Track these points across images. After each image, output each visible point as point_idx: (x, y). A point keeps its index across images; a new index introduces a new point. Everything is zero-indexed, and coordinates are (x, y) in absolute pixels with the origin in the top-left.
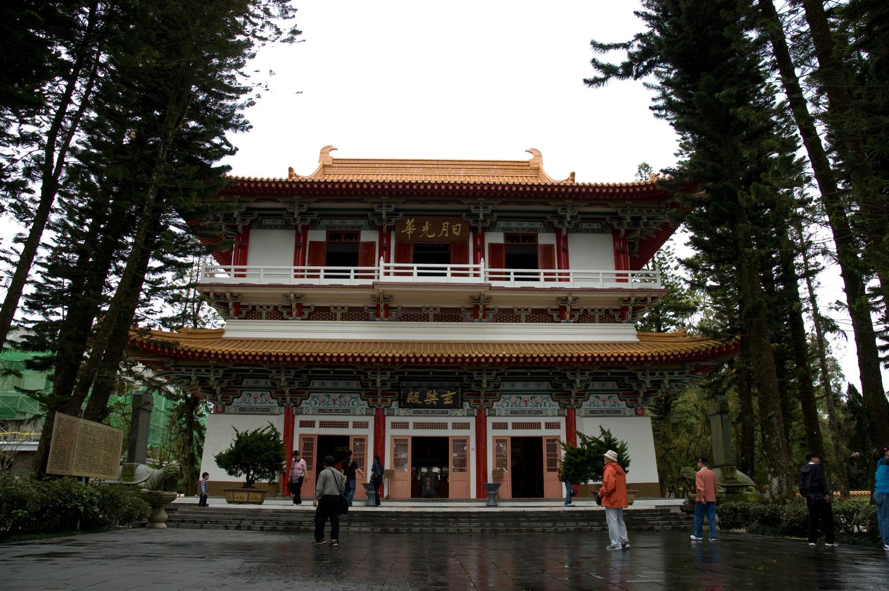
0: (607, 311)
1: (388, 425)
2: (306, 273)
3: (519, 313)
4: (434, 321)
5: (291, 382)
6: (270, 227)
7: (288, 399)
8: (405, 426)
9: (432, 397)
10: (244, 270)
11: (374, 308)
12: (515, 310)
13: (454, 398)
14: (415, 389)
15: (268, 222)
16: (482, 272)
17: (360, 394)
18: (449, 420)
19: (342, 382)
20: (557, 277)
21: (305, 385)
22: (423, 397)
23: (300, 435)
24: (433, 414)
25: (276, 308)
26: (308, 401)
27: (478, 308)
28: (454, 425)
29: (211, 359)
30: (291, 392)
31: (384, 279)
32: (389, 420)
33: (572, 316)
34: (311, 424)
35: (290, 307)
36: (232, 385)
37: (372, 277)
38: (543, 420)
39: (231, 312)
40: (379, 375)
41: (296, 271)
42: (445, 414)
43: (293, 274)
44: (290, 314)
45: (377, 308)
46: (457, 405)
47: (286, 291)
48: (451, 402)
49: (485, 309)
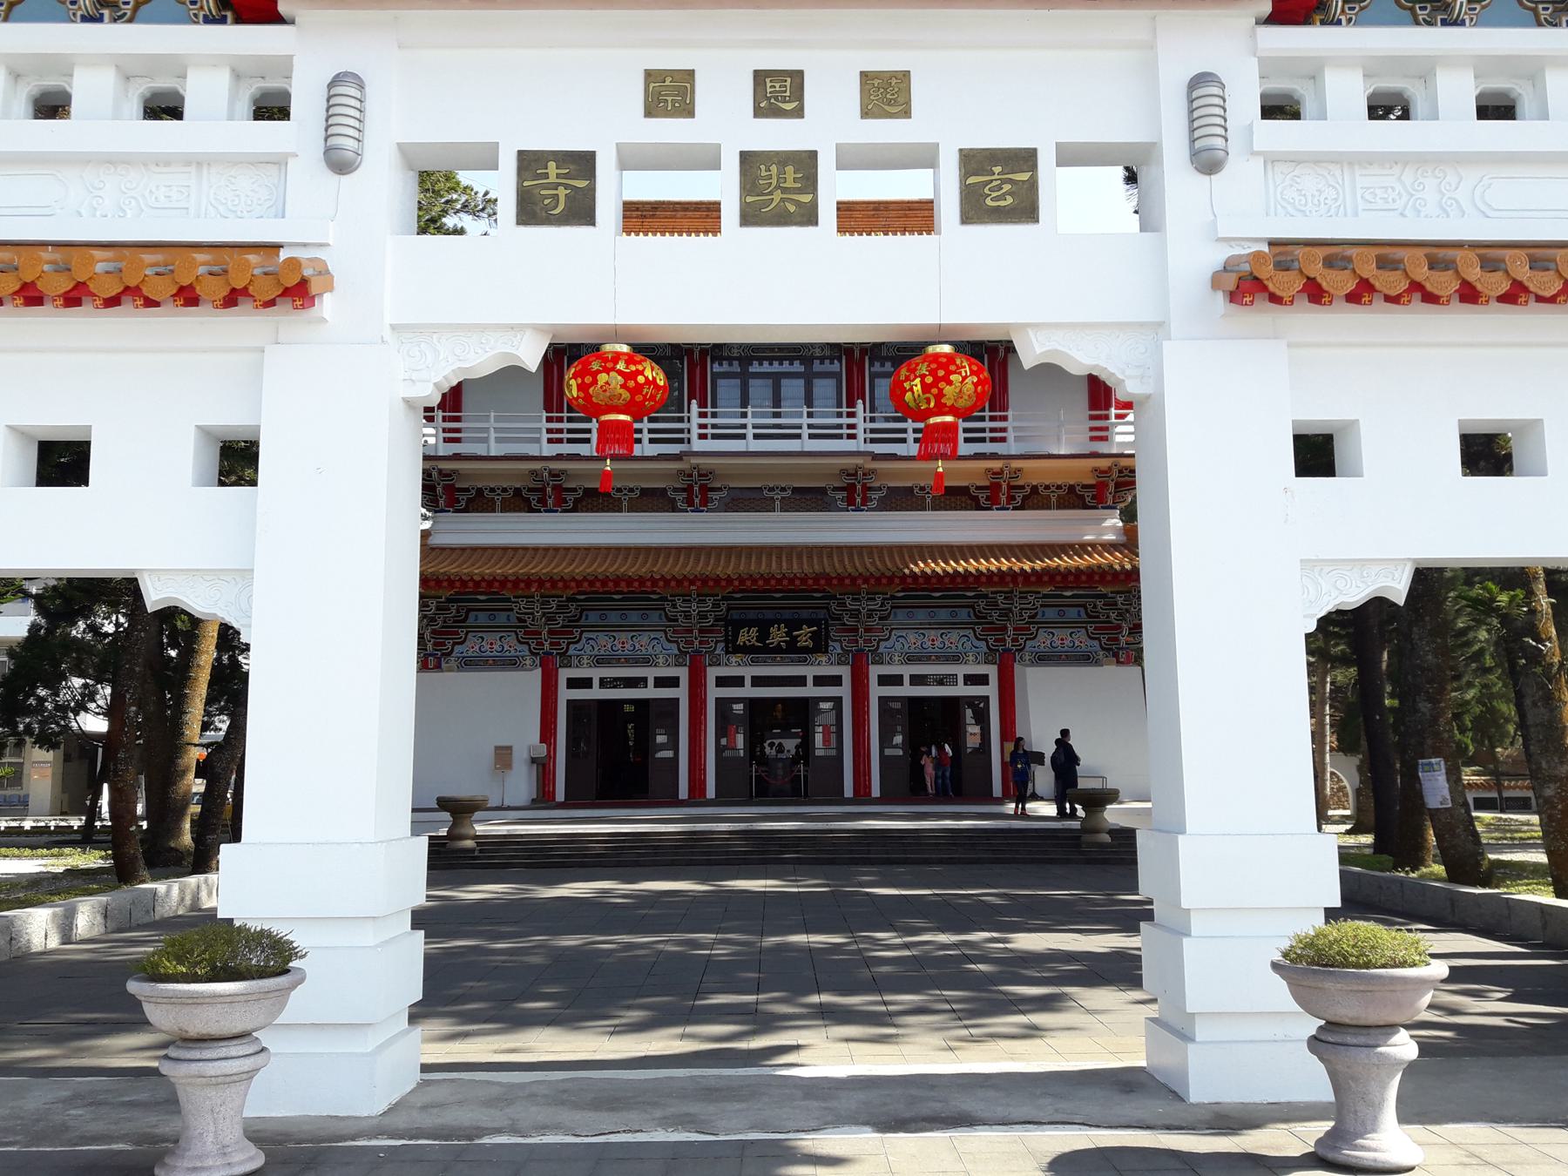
1: (562, 683)
2: (565, 436)
3: (492, 495)
5: (550, 619)
7: (547, 645)
8: (738, 681)
9: (778, 635)
10: (458, 430)
11: (684, 490)
13: (815, 637)
14: (750, 624)
16: (860, 432)
18: (809, 672)
19: (481, 615)
20: (845, 431)
21: (574, 622)
22: (764, 635)
24: (782, 663)
25: (518, 491)
26: (578, 646)
27: (853, 489)
28: (815, 678)
30: (551, 632)
31: (698, 445)
32: (712, 673)
33: (1011, 498)
34: (896, 680)
35: (543, 490)
36: (450, 623)
37: (680, 441)
38: (650, 673)
39: (441, 502)
40: (694, 606)
41: (549, 431)
42: (803, 662)
43: (545, 436)
44: (542, 501)
45: (689, 490)
46: (819, 646)
47: (537, 466)
48: (810, 644)
49: (866, 489)
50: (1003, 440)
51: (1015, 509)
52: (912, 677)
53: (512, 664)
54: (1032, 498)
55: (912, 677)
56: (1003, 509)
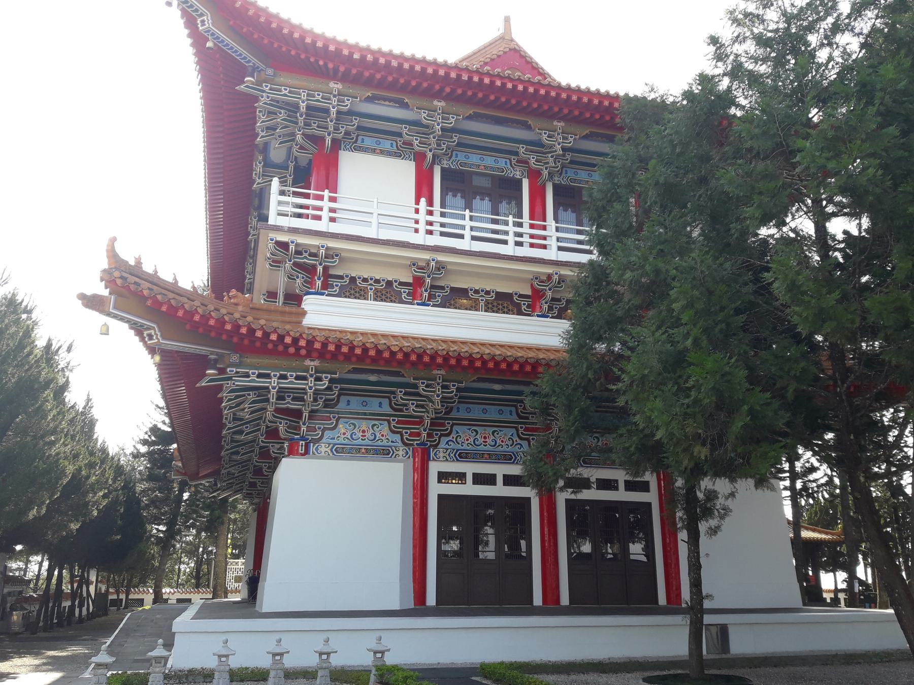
0: (389, 283)
3: (364, 285)
4: (375, 300)
6: (373, 151)
12: (470, 293)
15: (369, 142)
17: (517, 429)
19: (376, 401)
23: (440, 497)
29: (439, 366)
33: (325, 286)
50: (544, 247)
51: (552, 317)
52: (616, 489)
53: (384, 453)
54: (455, 298)
55: (616, 489)
56: (424, 304)
